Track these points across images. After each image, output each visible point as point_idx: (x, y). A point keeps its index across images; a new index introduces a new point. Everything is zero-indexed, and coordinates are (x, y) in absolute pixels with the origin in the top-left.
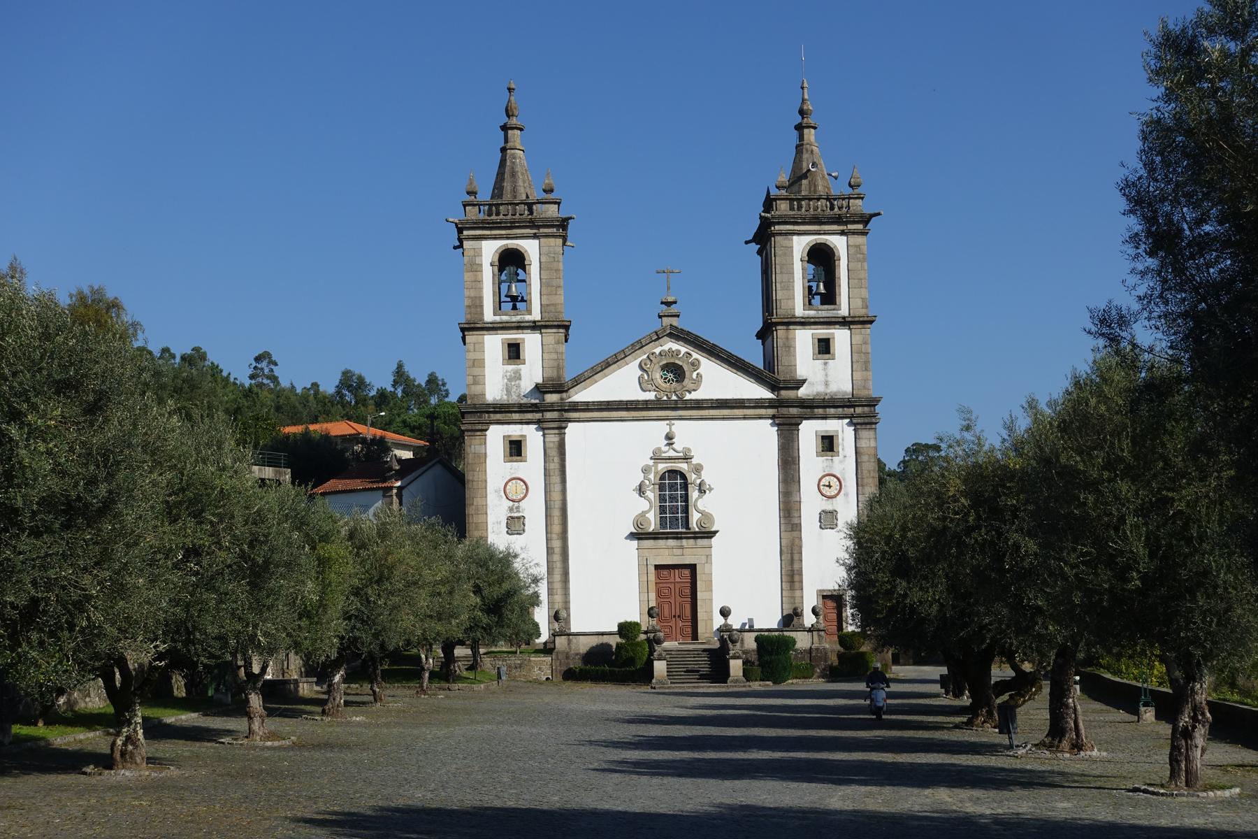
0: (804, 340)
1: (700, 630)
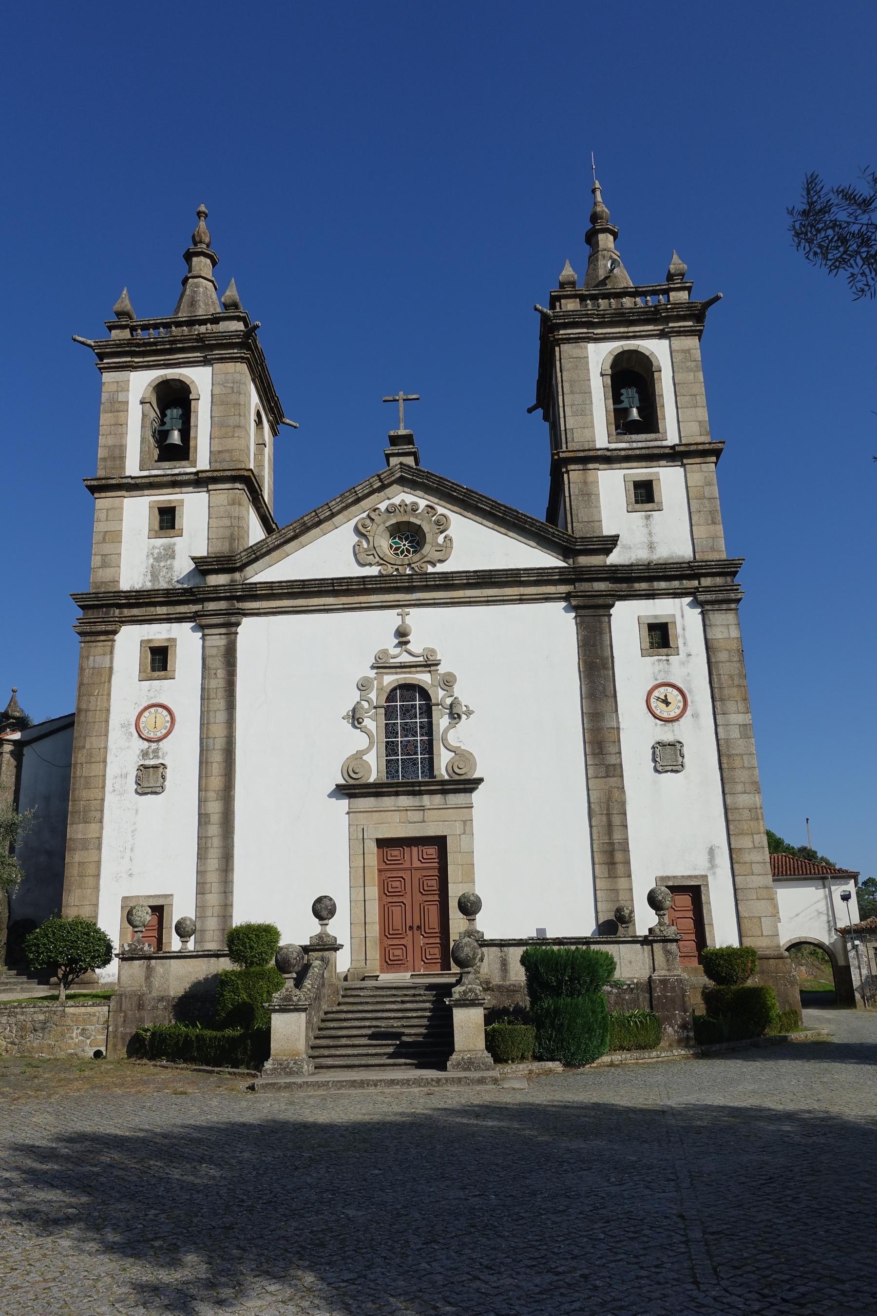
0: (611, 485)
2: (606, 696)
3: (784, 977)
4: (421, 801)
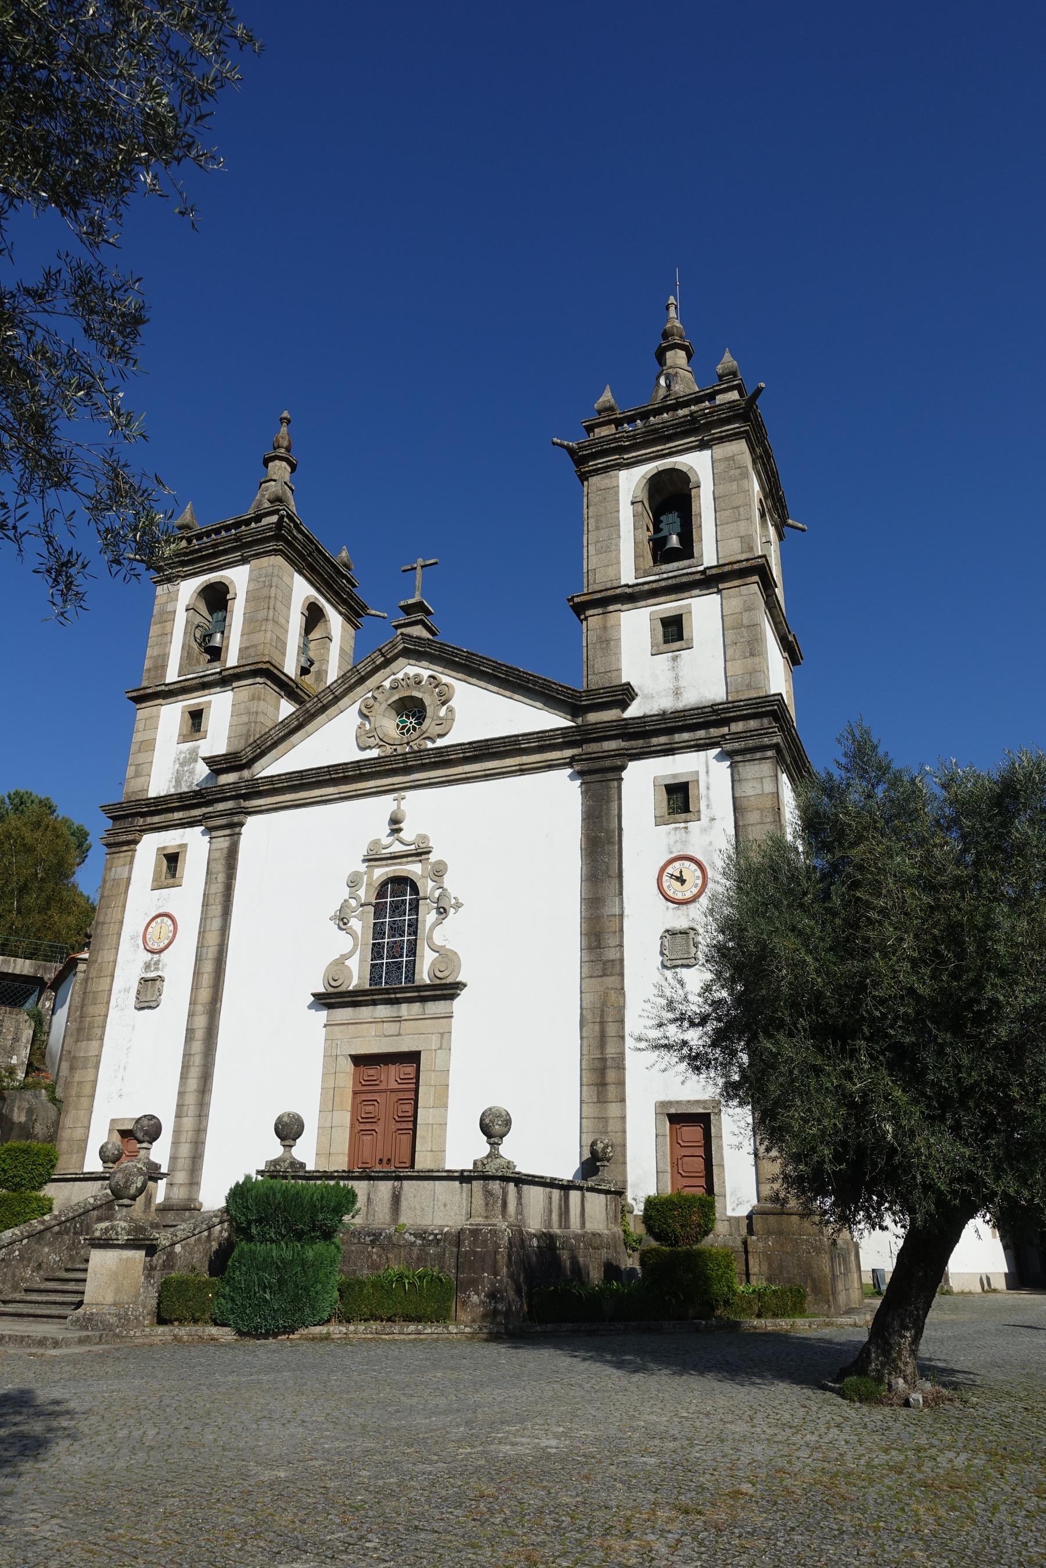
3: (807, 1240)
4: (399, 1010)
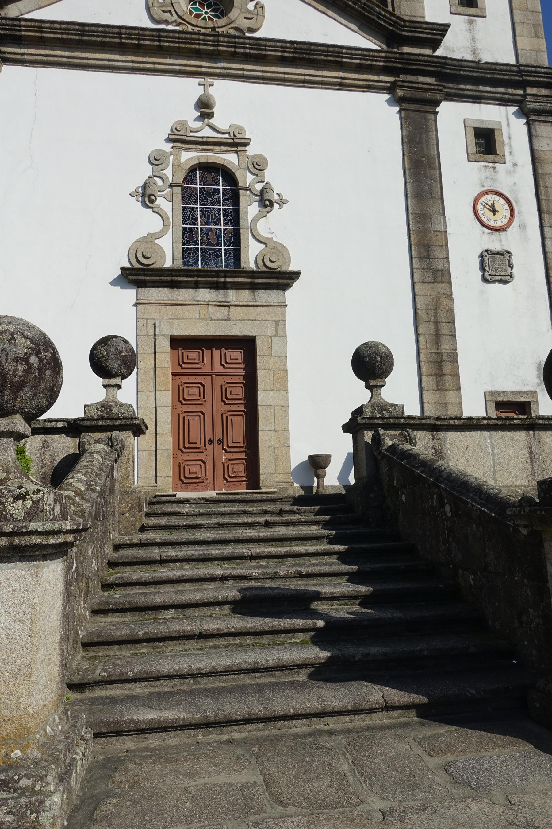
1: (263, 469)
2: (433, 197)
4: (225, 295)
